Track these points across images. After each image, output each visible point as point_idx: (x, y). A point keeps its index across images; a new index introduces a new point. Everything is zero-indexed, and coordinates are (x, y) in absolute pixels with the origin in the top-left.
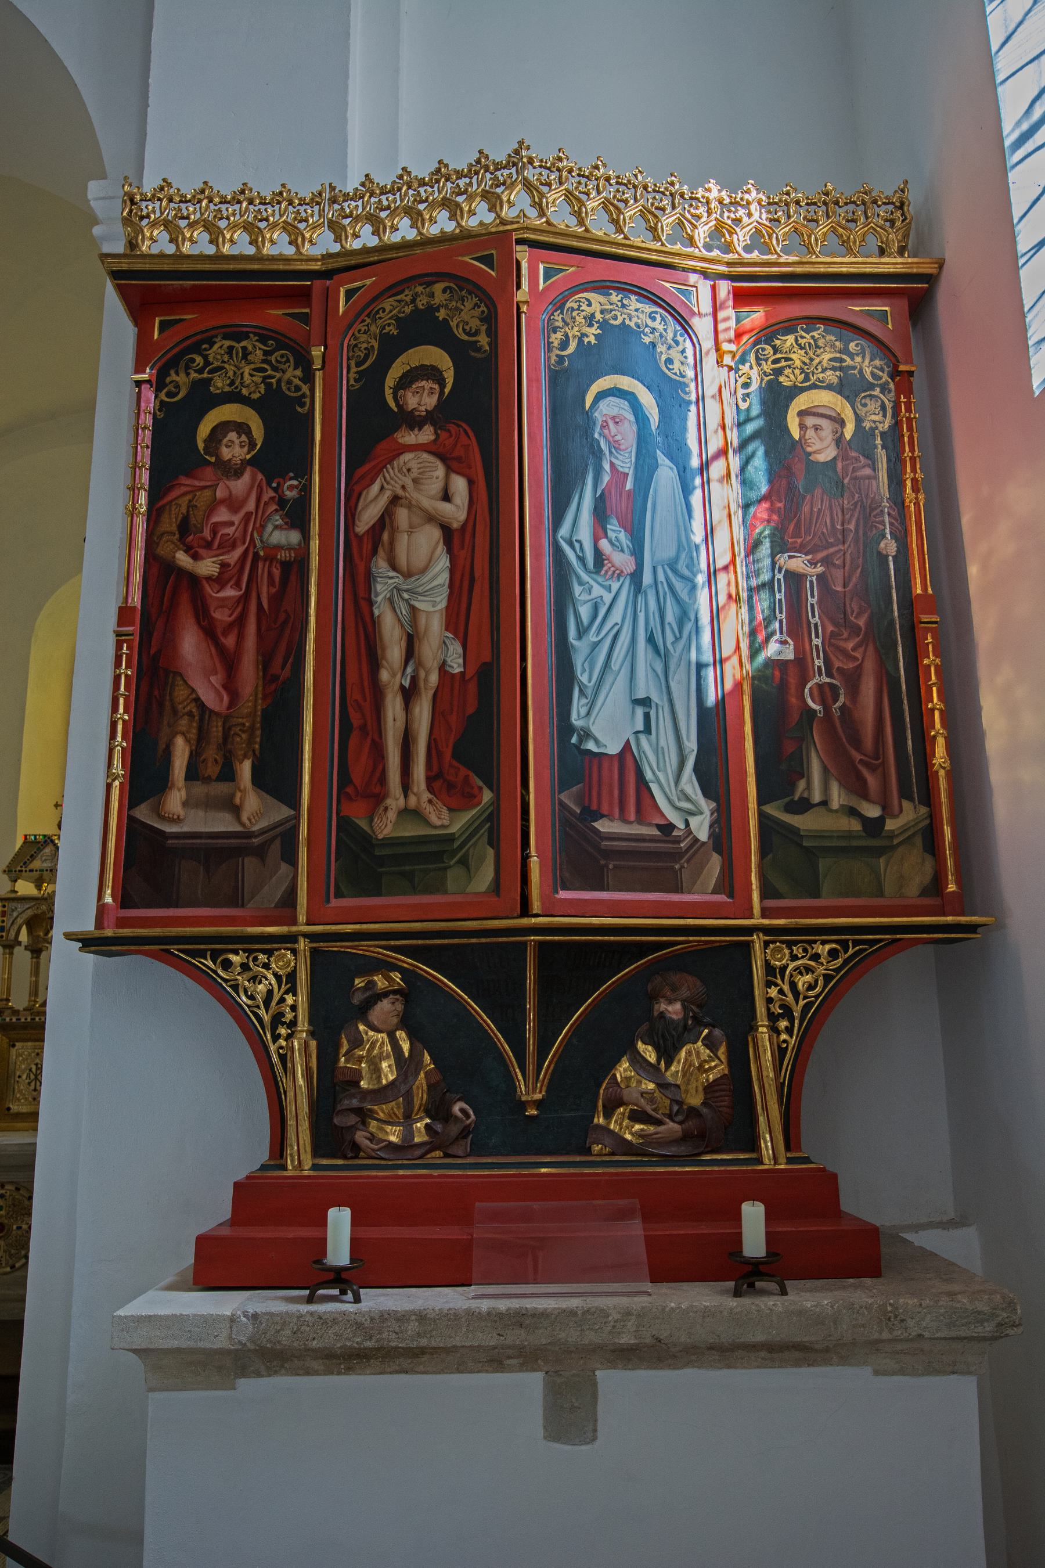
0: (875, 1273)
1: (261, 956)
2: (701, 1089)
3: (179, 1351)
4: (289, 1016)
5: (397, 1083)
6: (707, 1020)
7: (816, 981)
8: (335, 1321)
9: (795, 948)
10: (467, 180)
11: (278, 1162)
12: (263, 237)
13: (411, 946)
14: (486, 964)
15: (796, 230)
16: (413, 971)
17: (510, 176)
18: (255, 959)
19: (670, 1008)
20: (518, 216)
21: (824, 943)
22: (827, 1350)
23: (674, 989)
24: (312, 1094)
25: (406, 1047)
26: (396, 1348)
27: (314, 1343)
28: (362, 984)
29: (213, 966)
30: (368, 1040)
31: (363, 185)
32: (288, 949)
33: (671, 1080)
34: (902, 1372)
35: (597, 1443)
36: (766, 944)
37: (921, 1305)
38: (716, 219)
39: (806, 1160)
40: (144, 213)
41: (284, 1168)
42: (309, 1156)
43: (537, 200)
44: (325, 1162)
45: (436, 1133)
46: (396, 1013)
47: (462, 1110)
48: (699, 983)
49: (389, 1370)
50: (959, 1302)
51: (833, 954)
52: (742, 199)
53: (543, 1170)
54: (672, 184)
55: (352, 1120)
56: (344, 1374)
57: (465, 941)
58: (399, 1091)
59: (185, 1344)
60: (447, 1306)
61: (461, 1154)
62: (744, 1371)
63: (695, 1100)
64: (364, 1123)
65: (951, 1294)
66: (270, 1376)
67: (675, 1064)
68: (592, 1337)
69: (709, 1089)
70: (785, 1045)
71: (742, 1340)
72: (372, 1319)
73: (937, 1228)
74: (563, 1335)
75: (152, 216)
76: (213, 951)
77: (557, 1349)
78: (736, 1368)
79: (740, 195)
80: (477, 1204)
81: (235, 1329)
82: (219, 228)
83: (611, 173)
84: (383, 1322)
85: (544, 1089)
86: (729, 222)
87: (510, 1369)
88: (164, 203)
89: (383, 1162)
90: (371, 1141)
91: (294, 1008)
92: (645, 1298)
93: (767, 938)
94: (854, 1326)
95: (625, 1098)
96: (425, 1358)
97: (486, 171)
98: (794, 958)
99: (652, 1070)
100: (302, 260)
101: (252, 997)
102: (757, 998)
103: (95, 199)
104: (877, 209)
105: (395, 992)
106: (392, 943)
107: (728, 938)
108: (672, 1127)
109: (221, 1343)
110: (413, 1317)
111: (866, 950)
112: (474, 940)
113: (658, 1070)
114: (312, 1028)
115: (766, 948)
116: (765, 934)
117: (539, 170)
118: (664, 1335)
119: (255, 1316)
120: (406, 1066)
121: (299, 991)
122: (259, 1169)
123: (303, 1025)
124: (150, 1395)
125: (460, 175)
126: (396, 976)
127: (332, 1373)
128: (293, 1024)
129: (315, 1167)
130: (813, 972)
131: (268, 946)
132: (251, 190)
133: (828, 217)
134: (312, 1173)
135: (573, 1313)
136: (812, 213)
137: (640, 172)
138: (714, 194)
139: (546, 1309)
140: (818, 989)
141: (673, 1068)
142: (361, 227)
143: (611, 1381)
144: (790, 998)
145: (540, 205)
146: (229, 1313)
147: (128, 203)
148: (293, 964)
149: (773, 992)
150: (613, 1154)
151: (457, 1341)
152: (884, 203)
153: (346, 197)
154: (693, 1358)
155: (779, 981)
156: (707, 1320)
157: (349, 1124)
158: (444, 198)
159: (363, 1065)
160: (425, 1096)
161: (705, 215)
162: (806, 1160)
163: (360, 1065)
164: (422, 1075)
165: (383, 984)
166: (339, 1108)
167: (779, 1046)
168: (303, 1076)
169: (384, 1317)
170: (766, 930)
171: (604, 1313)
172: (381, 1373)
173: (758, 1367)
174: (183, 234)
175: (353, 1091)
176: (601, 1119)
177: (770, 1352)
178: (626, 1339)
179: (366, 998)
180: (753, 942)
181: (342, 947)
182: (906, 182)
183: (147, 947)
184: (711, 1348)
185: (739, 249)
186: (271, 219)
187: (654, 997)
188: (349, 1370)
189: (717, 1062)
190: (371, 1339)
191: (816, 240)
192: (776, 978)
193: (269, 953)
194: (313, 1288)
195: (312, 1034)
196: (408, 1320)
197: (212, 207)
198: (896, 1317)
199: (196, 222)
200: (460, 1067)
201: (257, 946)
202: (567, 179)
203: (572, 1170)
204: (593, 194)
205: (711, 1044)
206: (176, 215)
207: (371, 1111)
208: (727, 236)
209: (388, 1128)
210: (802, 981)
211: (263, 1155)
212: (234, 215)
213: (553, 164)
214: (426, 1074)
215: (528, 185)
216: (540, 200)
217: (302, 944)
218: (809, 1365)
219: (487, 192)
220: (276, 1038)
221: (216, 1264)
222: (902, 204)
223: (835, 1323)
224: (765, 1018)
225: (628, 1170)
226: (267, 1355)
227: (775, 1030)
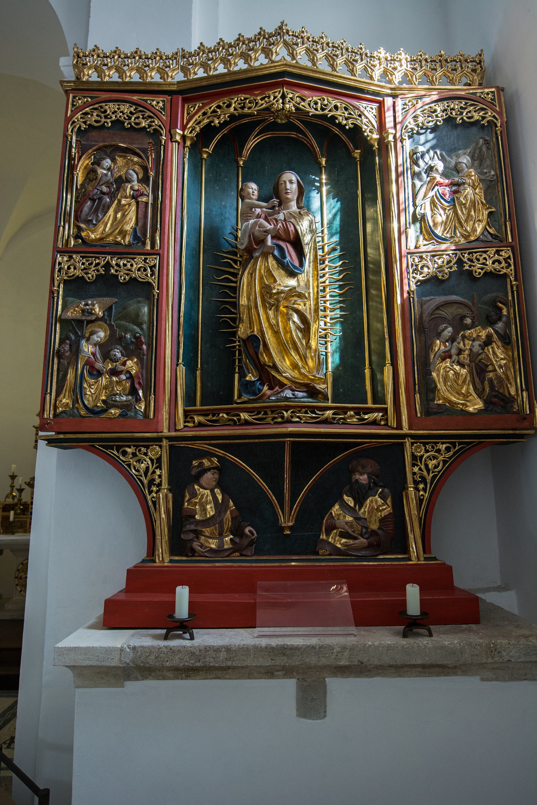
0: (477, 621)
1: (143, 449)
2: (377, 520)
3: (91, 666)
4: (158, 481)
5: (215, 517)
6: (381, 484)
7: (439, 464)
8: (179, 651)
9: (427, 446)
10: (254, 43)
11: (151, 558)
12: (147, 74)
13: (224, 444)
14: (264, 453)
15: (425, 74)
16: (224, 457)
17: (277, 40)
18: (140, 450)
19: (361, 478)
20: (281, 59)
21: (443, 443)
22: (455, 667)
23: (363, 467)
24: (170, 523)
25: (220, 497)
26: (214, 666)
27: (168, 663)
28: (197, 464)
29: (117, 454)
30: (200, 494)
31: (199, 48)
32: (157, 445)
33: (362, 516)
34: (497, 679)
35: (326, 719)
36: (412, 444)
37: (509, 643)
38: (384, 67)
39: (435, 559)
40: (84, 62)
41: (154, 562)
42: (168, 555)
43: (291, 51)
44: (176, 558)
45: (236, 543)
46: (214, 479)
47: (250, 531)
48: (376, 464)
49: (210, 677)
50: (531, 642)
51: (448, 449)
52: (397, 58)
53: (293, 564)
54: (361, 49)
55: (191, 536)
56: (185, 679)
57: (252, 441)
58: (216, 521)
59: (94, 663)
60: (243, 643)
61: (249, 554)
62: (408, 679)
63: (374, 526)
64: (198, 538)
65: (526, 637)
66: (143, 680)
67: (364, 507)
68: (324, 661)
69: (382, 520)
70: (422, 497)
71: (409, 663)
72: (200, 650)
73: (494, 591)
74: (308, 660)
75: (89, 64)
76: (117, 446)
77: (304, 666)
78: (403, 677)
79: (396, 56)
80: (259, 582)
81: (123, 655)
82: (123, 70)
83: (329, 40)
84: (206, 652)
85: (294, 520)
86: (391, 69)
87: (278, 677)
88: (95, 57)
89: (207, 559)
90: (201, 547)
91: (160, 476)
92: (352, 638)
93: (413, 441)
94: (472, 655)
95: (337, 526)
96: (230, 671)
97: (264, 38)
98: (427, 451)
99: (352, 510)
100: (166, 84)
101: (138, 471)
102: (407, 472)
103: (63, 66)
104: (467, 64)
105: (214, 468)
106: (213, 442)
107: (392, 441)
108: (362, 541)
109: (115, 663)
110: (223, 650)
111: (465, 447)
112: (257, 441)
113: (355, 510)
114: (170, 487)
115: (412, 446)
116: (411, 439)
117: (291, 37)
118: (365, 660)
119: (134, 648)
120: (220, 508)
121: (163, 467)
122: (141, 562)
123: (165, 485)
124: (76, 689)
125: (250, 40)
126: (215, 460)
127: (178, 679)
128: (159, 485)
129: (171, 561)
130: (437, 459)
131: (147, 444)
132: (141, 51)
133: (442, 68)
134: (169, 564)
135: (313, 647)
136: (434, 65)
137: (344, 41)
138: (382, 55)
139: (298, 645)
140: (440, 468)
141: (363, 510)
142: (198, 69)
143: (335, 686)
144: (425, 473)
145: (293, 54)
146: (119, 646)
147: (76, 57)
148: (160, 453)
149: (416, 469)
150: (330, 555)
151: (248, 663)
152: (471, 61)
153: (191, 55)
154: (380, 671)
155: (419, 464)
156: (389, 652)
157: (189, 538)
158: (242, 52)
159: (197, 507)
160: (230, 524)
161: (378, 65)
162: (435, 559)
163: (195, 507)
164: (229, 512)
165: (208, 464)
166: (184, 529)
167: (419, 498)
168: (164, 513)
169: (207, 649)
170: (412, 436)
171: (330, 648)
172: (206, 679)
173: (416, 677)
174: (105, 73)
175: (192, 520)
176: (324, 536)
177: (423, 668)
178: (343, 662)
179: (199, 472)
180: (405, 442)
181: (186, 444)
182: (482, 51)
183: (82, 444)
184: (391, 666)
185: (396, 83)
186: (151, 66)
187: (353, 472)
188: (188, 677)
189: (386, 506)
190: (199, 661)
191: (436, 79)
192: (417, 462)
193: (147, 447)
194: (170, 630)
195: (170, 490)
196: (220, 651)
197: (120, 59)
198: (496, 650)
199: (111, 67)
200: (248, 506)
201: (141, 444)
202: (307, 43)
203: (309, 564)
204: (320, 51)
205: (383, 497)
206: (101, 63)
207: (201, 531)
208: (390, 76)
209: (210, 541)
210: (431, 464)
211: (143, 554)
212: (132, 63)
213: (299, 34)
214: (231, 511)
215: (286, 44)
216: (293, 52)
217: (165, 443)
218: (445, 676)
219: (265, 48)
220: (150, 492)
221: (115, 615)
222: (480, 61)
223: (461, 653)
224: (412, 483)
225: (339, 564)
226: (141, 668)
227: (417, 489)
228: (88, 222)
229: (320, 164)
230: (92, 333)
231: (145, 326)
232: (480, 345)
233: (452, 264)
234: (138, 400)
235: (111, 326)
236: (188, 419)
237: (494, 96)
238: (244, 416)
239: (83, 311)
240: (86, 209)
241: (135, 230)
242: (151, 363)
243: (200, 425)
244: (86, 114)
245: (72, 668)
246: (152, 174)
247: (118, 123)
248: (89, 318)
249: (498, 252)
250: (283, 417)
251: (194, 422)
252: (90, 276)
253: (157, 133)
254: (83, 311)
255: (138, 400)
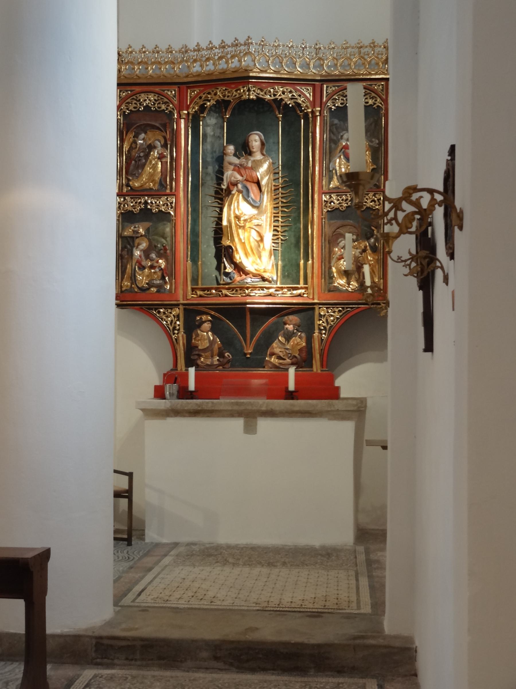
4: (178, 328)
36: (320, 308)
41: (177, 370)
47: (228, 355)
69: (300, 350)
123: (182, 330)
128: (179, 330)
182: (387, 40)
193: (171, 309)
195: (184, 333)
228: (133, 175)
229: (278, 118)
230: (139, 244)
231: (169, 239)
232: (359, 252)
233: (348, 201)
234: (166, 283)
235: (149, 240)
236: (194, 293)
237: (383, 87)
238: (224, 292)
239: (133, 231)
240: (131, 168)
241: (160, 180)
242: (172, 262)
243: (201, 296)
244: (128, 103)
245: (143, 410)
246: (169, 142)
247: (147, 107)
248: (137, 235)
249: (374, 195)
250: (245, 293)
251: (197, 295)
252: (136, 210)
253: (171, 113)
254: (133, 231)
255: (166, 283)
